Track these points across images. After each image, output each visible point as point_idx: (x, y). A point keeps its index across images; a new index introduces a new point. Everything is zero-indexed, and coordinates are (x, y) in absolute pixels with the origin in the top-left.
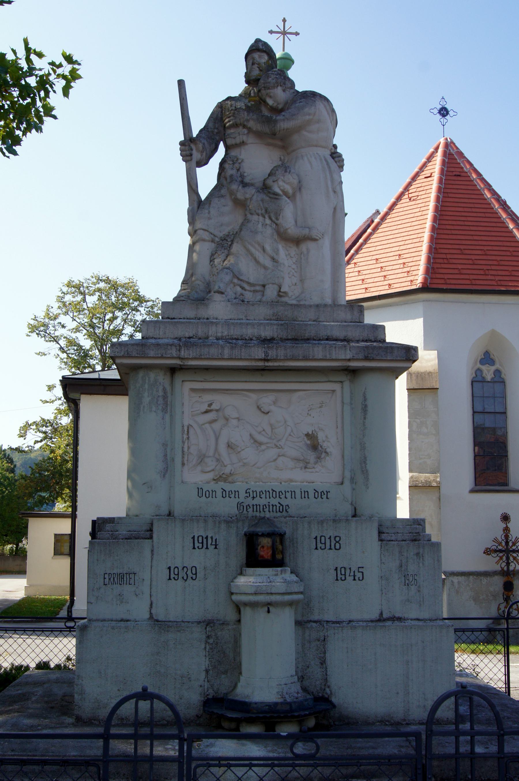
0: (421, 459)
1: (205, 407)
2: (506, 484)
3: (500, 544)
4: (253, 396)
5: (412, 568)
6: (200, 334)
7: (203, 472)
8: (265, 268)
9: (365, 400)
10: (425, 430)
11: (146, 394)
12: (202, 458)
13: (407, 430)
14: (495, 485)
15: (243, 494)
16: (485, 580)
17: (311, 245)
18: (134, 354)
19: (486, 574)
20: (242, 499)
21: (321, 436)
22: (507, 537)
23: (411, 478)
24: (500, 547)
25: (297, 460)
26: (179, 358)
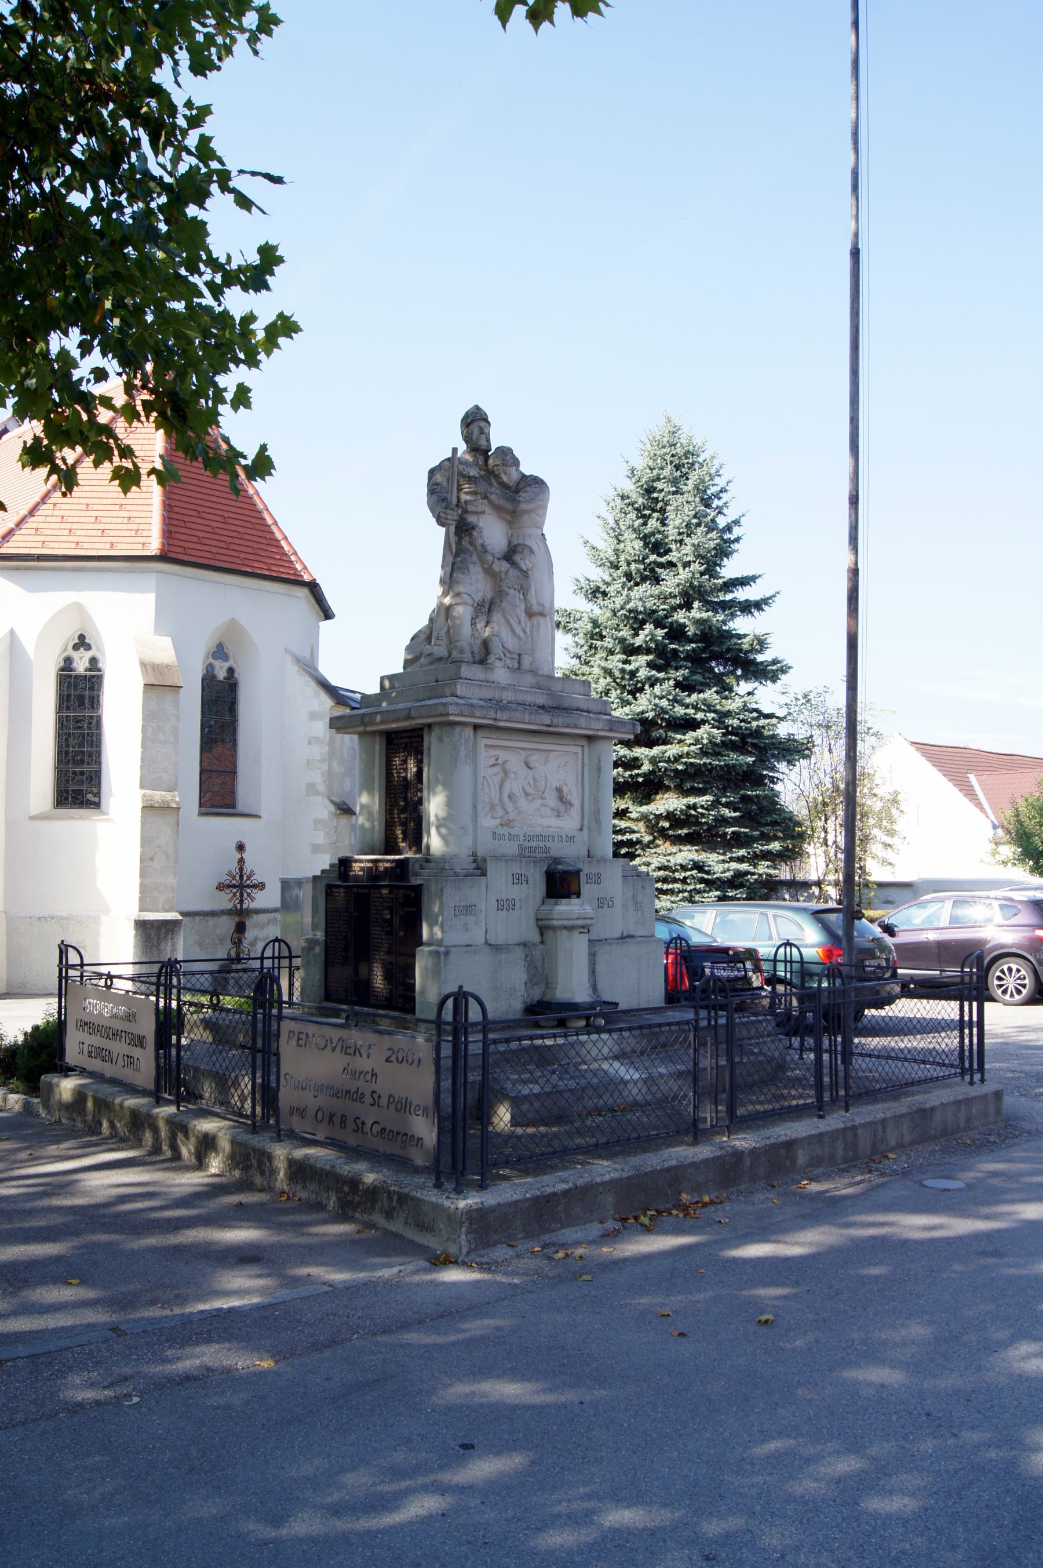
0: (155, 772)
1: (492, 761)
2: (233, 807)
3: (234, 878)
4: (523, 753)
5: (639, 897)
6: (497, 697)
7: (493, 818)
8: (519, 638)
9: (599, 762)
10: (162, 737)
11: (462, 748)
12: (493, 808)
13: (140, 736)
14: (221, 807)
15: (522, 838)
16: (212, 921)
17: (541, 620)
18: (466, 713)
19: (213, 914)
20: (521, 842)
21: (565, 789)
22: (241, 869)
23: (144, 795)
24: (234, 882)
25: (553, 809)
26: (495, 719)
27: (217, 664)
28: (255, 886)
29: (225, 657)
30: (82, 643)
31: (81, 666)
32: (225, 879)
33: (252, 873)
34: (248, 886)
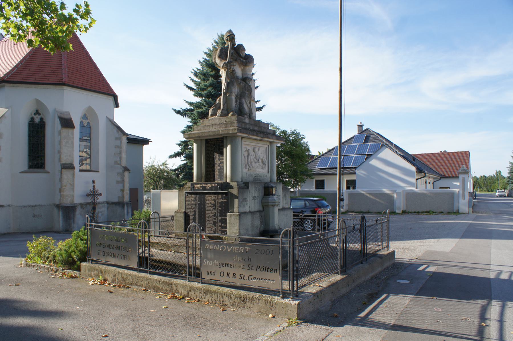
22: (94, 189)
27: (84, 121)
28: (98, 195)
29: (87, 119)
30: (37, 113)
31: (37, 119)
32: (88, 192)
33: (97, 190)
34: (96, 195)
